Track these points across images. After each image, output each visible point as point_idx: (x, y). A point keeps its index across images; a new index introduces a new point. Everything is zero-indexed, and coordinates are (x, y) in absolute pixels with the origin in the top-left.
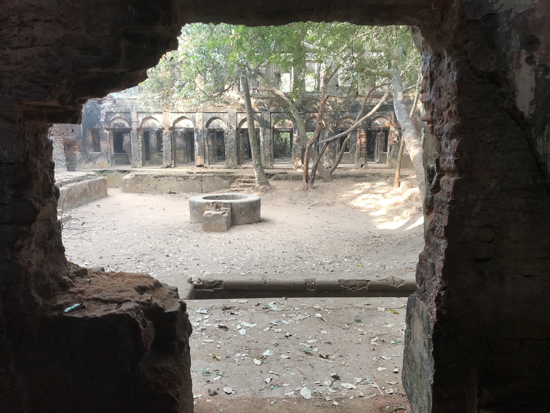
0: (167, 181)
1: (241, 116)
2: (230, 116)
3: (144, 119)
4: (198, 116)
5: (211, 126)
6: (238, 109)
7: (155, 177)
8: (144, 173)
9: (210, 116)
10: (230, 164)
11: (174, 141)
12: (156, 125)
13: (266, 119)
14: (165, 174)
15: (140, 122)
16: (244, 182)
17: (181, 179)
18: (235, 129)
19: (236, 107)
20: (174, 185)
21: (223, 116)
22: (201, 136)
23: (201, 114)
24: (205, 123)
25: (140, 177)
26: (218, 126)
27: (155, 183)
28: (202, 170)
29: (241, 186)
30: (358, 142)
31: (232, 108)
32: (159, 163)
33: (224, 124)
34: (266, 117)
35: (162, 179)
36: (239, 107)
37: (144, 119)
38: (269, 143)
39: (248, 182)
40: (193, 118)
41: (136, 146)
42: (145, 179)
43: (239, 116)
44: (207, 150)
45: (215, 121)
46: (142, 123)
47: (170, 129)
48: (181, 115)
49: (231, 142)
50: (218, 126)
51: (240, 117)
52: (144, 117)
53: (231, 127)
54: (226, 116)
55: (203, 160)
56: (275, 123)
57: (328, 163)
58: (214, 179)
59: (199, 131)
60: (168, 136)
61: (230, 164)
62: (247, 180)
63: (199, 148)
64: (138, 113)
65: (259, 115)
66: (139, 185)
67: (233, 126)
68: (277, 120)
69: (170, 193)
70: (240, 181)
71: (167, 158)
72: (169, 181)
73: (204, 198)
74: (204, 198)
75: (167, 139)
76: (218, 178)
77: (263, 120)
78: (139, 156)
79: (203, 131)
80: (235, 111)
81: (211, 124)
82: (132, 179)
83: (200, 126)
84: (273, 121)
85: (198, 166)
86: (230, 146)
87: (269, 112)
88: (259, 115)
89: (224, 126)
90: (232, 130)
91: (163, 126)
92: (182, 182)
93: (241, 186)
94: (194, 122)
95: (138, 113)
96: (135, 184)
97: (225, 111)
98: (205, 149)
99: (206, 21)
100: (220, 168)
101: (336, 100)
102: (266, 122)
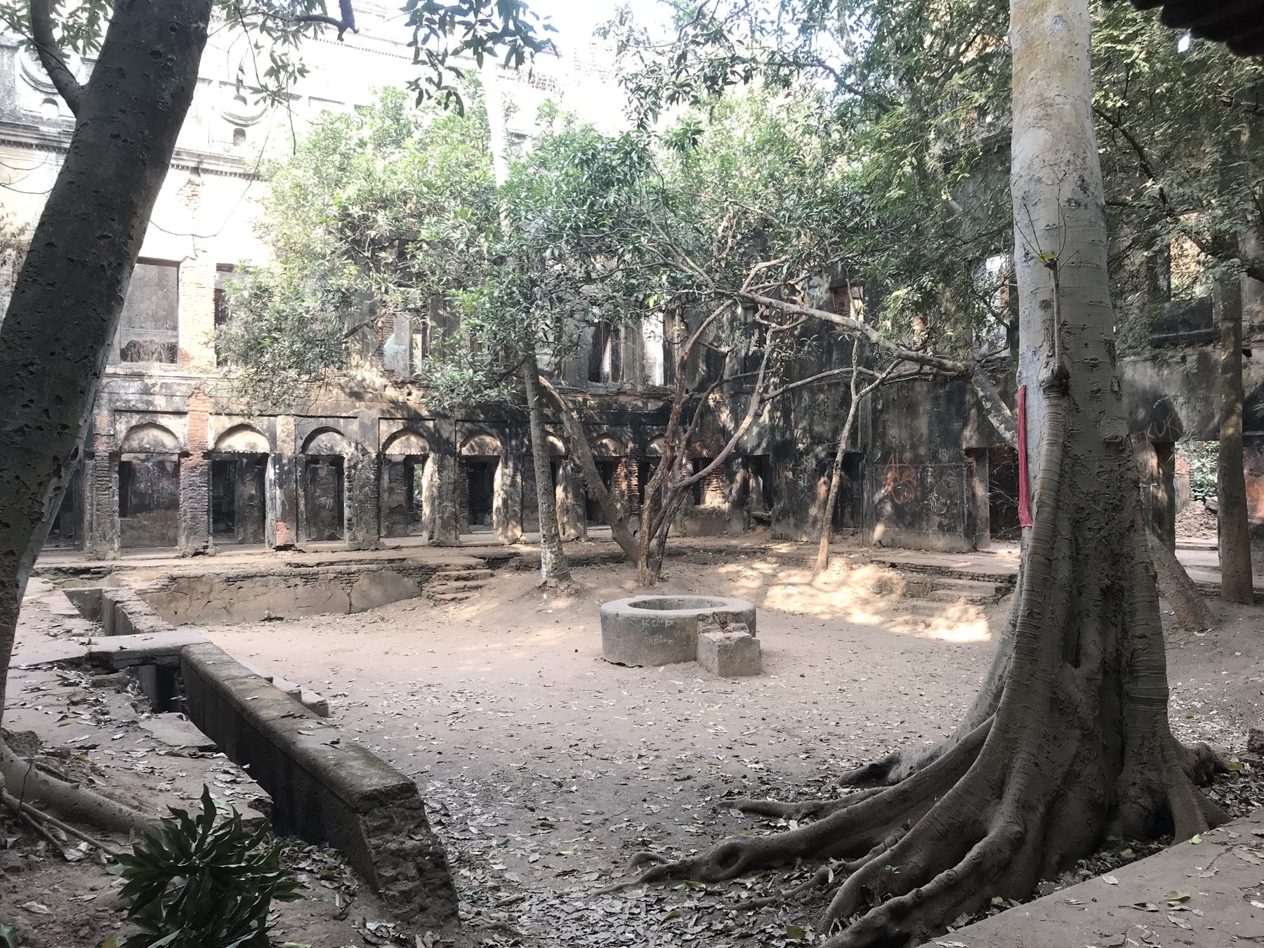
0: (261, 590)
1: (389, 426)
2: (363, 426)
3: (132, 430)
4: (284, 425)
5: (313, 449)
6: (383, 411)
7: (228, 580)
8: (200, 572)
9: (313, 425)
10: (360, 538)
11: (230, 489)
12: (164, 445)
13: (445, 435)
14: (254, 571)
15: (122, 436)
16: (458, 579)
17: (298, 581)
18: (374, 456)
19: (379, 406)
20: (279, 597)
21: (346, 426)
22: (290, 471)
23: (291, 419)
24: (300, 442)
25: (183, 582)
26: (332, 448)
27: (226, 595)
28: (288, 556)
29: (458, 590)
30: (624, 486)
31: (369, 408)
32: (258, 538)
33: (345, 444)
34: (447, 430)
35: (247, 584)
36: (385, 406)
37: (132, 428)
38: (451, 487)
39: (465, 579)
40: (269, 428)
41: (104, 499)
42: (201, 588)
43: (384, 426)
44: (302, 507)
45: (323, 437)
46: (127, 438)
47: (207, 455)
48: (238, 421)
49: (363, 487)
50: (332, 448)
51: (386, 429)
52: (134, 423)
53: (365, 452)
54: (354, 426)
55: (294, 533)
56: (463, 445)
57: (573, 531)
58: (380, 576)
59: (285, 461)
60: (202, 474)
61: (360, 538)
62: (464, 573)
63: (283, 503)
64: (117, 411)
65: (430, 424)
66: (182, 605)
67: (370, 450)
68: (468, 436)
69: (269, 619)
70: (448, 578)
71: (192, 531)
72: (264, 590)
73: (635, 605)
74: (635, 605)
75: (198, 480)
76: (390, 573)
77: (440, 436)
78: (113, 526)
79: (294, 461)
80: (375, 414)
81: (312, 445)
82: (161, 590)
83: (289, 449)
84: (460, 440)
85: (279, 548)
86: (361, 497)
87: (452, 421)
88: (430, 424)
89: (346, 449)
90: (366, 458)
91: (188, 448)
92: (300, 588)
93: (458, 590)
94: (273, 440)
95: (117, 411)
96: (170, 601)
97: (350, 414)
98: (297, 504)
99: (53, 190)
100: (317, 553)
101: (585, 400)
102: (447, 441)
